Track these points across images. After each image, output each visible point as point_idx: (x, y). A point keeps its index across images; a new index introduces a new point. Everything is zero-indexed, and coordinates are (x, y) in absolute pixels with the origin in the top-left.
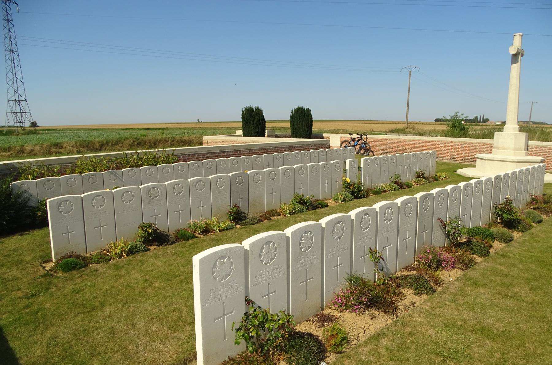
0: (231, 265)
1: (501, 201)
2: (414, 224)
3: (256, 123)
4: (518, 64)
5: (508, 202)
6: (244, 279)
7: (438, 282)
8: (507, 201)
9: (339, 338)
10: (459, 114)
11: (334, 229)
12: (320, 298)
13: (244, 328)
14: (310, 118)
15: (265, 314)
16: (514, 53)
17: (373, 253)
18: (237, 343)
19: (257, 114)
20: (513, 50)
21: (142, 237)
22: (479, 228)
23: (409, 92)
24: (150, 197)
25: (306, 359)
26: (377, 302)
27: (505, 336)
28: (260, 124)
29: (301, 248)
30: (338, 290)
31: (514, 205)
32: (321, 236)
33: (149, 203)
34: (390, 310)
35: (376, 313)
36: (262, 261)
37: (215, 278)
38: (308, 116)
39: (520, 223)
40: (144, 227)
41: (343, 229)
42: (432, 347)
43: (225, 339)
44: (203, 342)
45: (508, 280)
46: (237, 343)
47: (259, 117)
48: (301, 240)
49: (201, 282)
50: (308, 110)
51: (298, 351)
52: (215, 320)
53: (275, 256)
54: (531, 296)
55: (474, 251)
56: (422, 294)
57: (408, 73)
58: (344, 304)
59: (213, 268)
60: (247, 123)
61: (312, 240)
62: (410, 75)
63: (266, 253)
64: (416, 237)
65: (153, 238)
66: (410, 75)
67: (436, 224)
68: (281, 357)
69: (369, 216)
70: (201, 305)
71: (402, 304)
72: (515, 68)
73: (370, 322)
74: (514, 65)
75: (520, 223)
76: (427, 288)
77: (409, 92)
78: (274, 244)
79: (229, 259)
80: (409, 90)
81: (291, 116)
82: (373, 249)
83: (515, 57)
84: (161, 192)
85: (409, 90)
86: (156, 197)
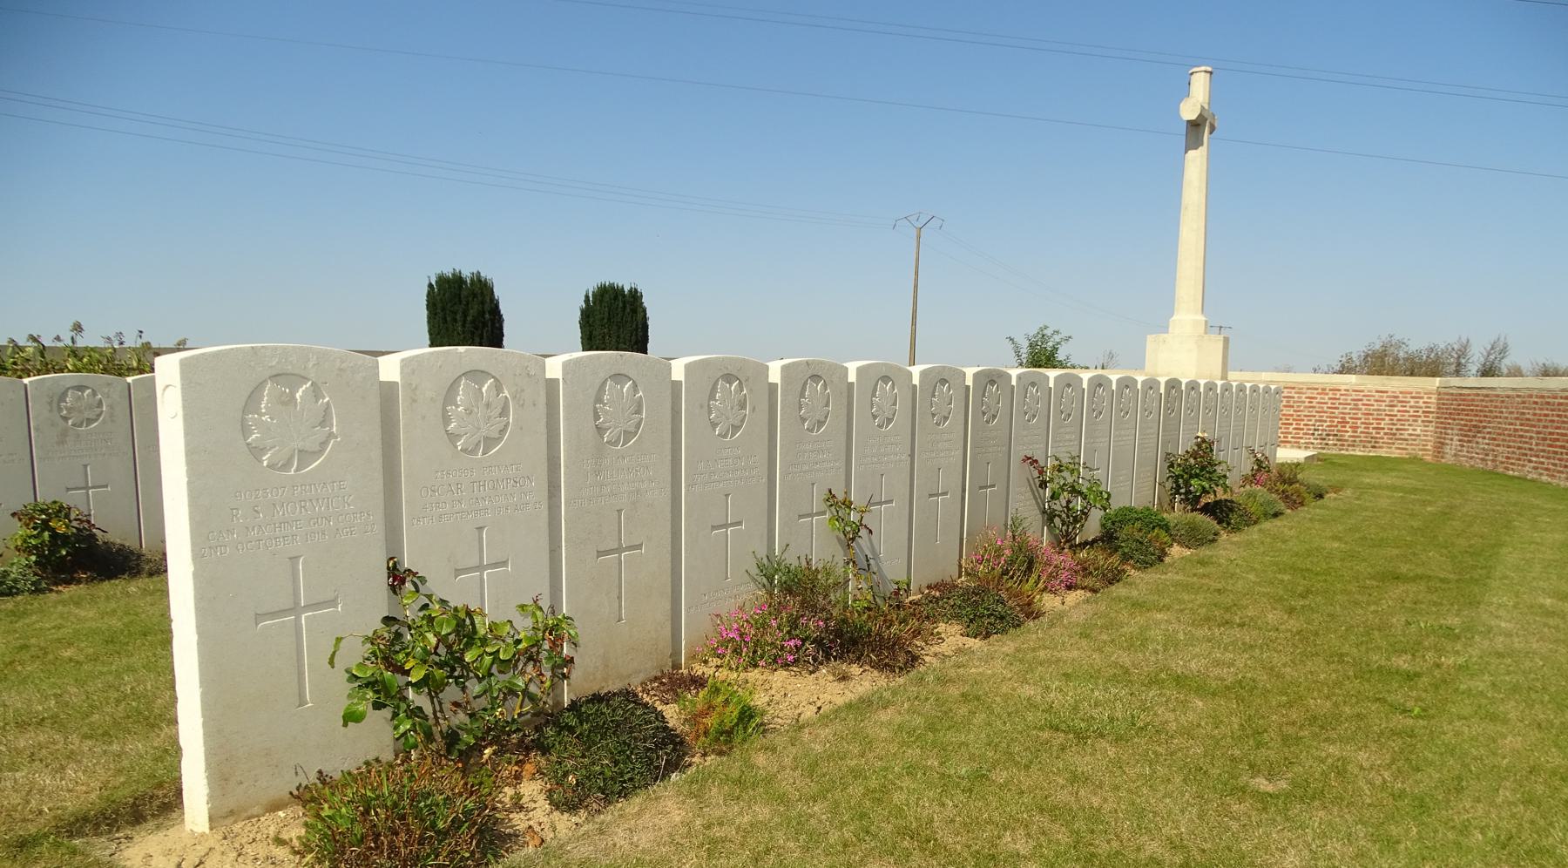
0: (325, 421)
1: (1184, 445)
2: (960, 452)
3: (473, 322)
4: (1203, 150)
5: (1204, 449)
6: (378, 485)
7: (1032, 613)
8: (1199, 445)
9: (733, 712)
10: (1048, 332)
11: (712, 397)
12: (668, 624)
13: (381, 681)
14: (640, 316)
15: (465, 628)
16: (1194, 117)
17: (838, 504)
18: (350, 717)
19: (475, 296)
20: (1189, 112)
21: (28, 550)
22: (1131, 510)
23: (916, 286)
24: (66, 419)
25: (616, 763)
26: (854, 642)
27: (1240, 690)
28: (484, 325)
29: (600, 430)
30: (727, 606)
31: (1217, 455)
32: (668, 405)
33: (62, 442)
34: (895, 659)
35: (855, 669)
36: (453, 437)
37: (256, 452)
38: (634, 311)
39: (1231, 510)
40: (42, 517)
41: (743, 406)
42: (1042, 717)
43: (302, 702)
44: (204, 696)
45: (1227, 600)
46: (350, 717)
47: (483, 303)
48: (599, 400)
49: (191, 452)
50: (635, 298)
51: (587, 742)
52: (259, 617)
53: (503, 431)
54: (1293, 624)
55: (1124, 554)
56: (987, 636)
57: (914, 232)
58: (749, 648)
59: (245, 410)
60: (445, 321)
61: (639, 412)
62: (919, 237)
63: (469, 411)
64: (963, 498)
65: (75, 553)
66: (919, 237)
67: (1020, 476)
68: (527, 766)
69: (825, 386)
70: (194, 544)
71: (931, 654)
72: (1196, 162)
73: (838, 687)
74: (1191, 153)
75: (1231, 510)
76: (1002, 618)
77: (916, 286)
78: (498, 388)
79: (316, 392)
80: (916, 280)
81: (582, 311)
82: (840, 497)
83: (1195, 126)
84: (111, 407)
85: (916, 280)
86: (90, 421)
